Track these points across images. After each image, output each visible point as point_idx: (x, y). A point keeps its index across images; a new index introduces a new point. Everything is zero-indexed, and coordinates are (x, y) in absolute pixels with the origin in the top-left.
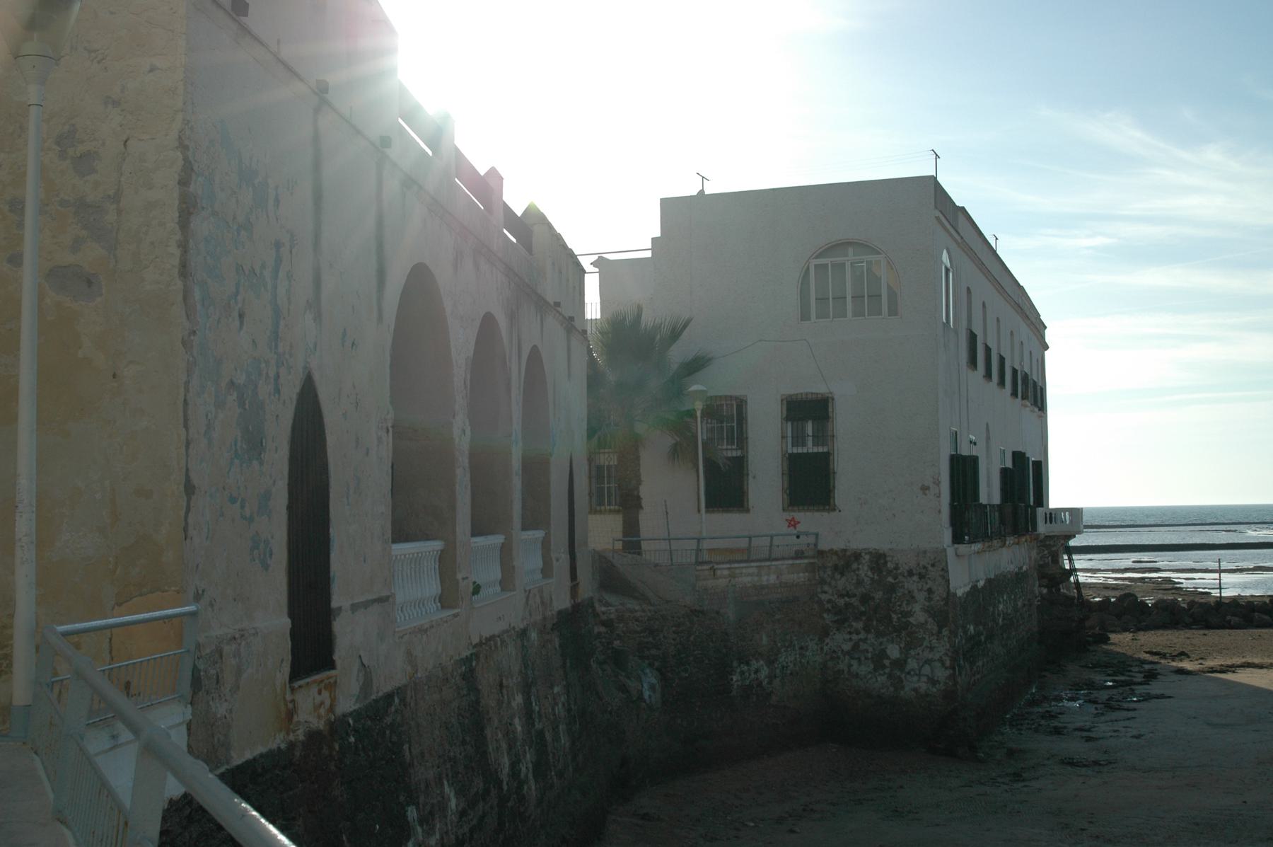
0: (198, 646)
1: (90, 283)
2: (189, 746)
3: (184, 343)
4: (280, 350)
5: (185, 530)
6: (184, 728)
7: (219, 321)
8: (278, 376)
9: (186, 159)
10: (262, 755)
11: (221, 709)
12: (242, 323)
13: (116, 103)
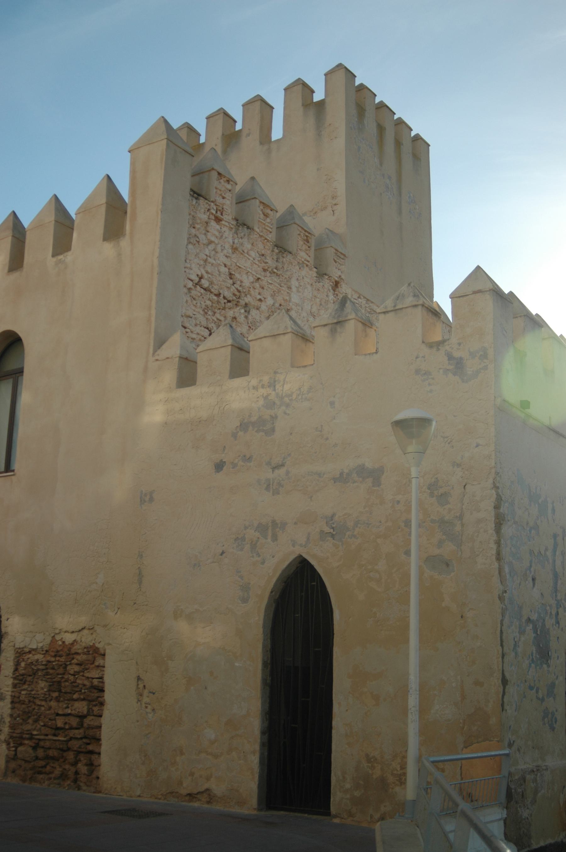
0: (510, 774)
1: (448, 565)
2: (505, 834)
3: (500, 598)
4: (559, 598)
5: (502, 705)
6: (502, 823)
7: (520, 584)
8: (557, 614)
9: (498, 494)
10: (551, 845)
11: (525, 814)
12: (534, 584)
13: (459, 465)
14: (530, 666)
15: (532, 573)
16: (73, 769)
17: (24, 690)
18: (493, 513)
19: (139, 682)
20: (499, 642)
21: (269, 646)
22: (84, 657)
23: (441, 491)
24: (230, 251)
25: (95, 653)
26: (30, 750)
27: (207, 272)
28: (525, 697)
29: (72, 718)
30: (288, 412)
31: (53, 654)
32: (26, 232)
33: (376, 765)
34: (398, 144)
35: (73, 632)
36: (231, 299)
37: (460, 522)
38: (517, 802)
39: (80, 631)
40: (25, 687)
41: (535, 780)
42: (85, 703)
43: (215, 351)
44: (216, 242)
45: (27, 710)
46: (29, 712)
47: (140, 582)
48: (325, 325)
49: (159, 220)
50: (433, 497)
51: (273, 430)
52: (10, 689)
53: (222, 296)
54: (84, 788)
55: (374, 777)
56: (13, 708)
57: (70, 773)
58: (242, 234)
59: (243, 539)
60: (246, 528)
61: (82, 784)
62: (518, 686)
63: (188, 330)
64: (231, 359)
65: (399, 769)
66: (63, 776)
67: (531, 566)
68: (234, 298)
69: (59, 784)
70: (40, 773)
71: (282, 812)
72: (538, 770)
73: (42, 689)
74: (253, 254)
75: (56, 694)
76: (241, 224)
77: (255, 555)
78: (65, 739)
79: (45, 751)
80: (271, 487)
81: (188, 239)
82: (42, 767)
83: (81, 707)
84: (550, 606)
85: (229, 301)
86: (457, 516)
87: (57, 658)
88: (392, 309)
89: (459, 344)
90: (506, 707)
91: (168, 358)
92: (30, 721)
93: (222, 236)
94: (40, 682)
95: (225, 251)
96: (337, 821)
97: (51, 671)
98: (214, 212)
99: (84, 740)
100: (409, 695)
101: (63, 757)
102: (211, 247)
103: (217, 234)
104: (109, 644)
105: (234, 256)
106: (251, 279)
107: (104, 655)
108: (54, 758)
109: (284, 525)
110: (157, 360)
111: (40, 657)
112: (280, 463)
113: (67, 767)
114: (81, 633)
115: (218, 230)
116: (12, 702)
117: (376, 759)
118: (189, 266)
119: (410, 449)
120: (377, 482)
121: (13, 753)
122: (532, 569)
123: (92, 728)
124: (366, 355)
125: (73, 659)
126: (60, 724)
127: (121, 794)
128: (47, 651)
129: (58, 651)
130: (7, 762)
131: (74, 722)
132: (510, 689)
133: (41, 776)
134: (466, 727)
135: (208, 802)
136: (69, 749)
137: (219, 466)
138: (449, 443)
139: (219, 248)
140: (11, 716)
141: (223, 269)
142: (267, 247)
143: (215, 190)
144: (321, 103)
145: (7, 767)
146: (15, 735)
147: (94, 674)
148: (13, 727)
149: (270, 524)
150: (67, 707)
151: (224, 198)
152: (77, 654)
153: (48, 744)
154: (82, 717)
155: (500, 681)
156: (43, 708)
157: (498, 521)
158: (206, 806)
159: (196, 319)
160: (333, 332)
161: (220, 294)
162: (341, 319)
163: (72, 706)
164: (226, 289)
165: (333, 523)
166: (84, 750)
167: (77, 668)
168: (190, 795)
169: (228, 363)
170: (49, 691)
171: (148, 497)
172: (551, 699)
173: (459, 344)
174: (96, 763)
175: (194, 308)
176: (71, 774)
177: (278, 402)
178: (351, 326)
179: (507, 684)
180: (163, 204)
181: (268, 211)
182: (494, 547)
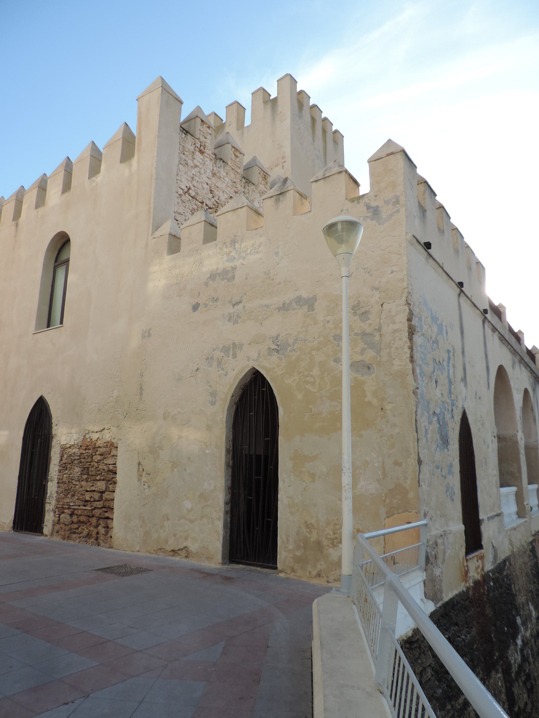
1: (369, 368)
3: (414, 393)
5: (419, 482)
6: (422, 583)
7: (427, 384)
8: (452, 410)
9: (410, 309)
10: (456, 595)
13: (377, 289)
14: (436, 450)
15: (435, 377)
16: (95, 531)
17: (65, 474)
18: (406, 324)
19: (140, 467)
20: (415, 429)
21: (231, 437)
22: (104, 449)
23: (363, 310)
24: (211, 175)
25: (112, 446)
26: (68, 517)
27: (194, 186)
28: (434, 475)
29: (95, 493)
30: (244, 263)
31: (84, 448)
32: (72, 166)
33: (313, 530)
34: (324, 131)
35: (97, 432)
36: (211, 207)
37: (378, 333)
38: (432, 564)
39: (101, 431)
40: (66, 472)
41: (443, 544)
42: (104, 482)
43: (193, 228)
44: (200, 166)
45: (67, 488)
46: (68, 490)
47: (141, 394)
48: (272, 197)
49: (157, 143)
50: (356, 315)
51: (234, 277)
52: (57, 473)
53: (205, 204)
54: (102, 544)
55: (312, 540)
56: (59, 487)
57: (93, 533)
58: (219, 165)
59: (212, 358)
60: (214, 350)
61: (101, 542)
62: (429, 466)
63: (178, 222)
64: (204, 231)
65: (332, 534)
66: (89, 535)
67: (434, 371)
68: (214, 206)
69: (86, 541)
70: (74, 533)
71: (241, 566)
72: (445, 534)
73: (77, 473)
74: (227, 179)
75: (86, 476)
76: (219, 158)
77: (220, 369)
78: (90, 508)
79: (78, 518)
80: (233, 319)
81: (179, 161)
82: (76, 529)
83: (101, 485)
84: (447, 403)
85: (210, 208)
86: (376, 329)
87: (87, 451)
88: (322, 177)
89: (376, 196)
90: (422, 483)
91: (161, 236)
92: (69, 496)
93: (204, 164)
94: (76, 468)
95: (207, 174)
96: (282, 575)
97: (83, 460)
98: (199, 146)
99: (103, 509)
100: (343, 474)
101: (89, 522)
102: (197, 169)
103: (201, 161)
104: (120, 440)
105: (213, 178)
106: (226, 196)
107: (117, 448)
108: (83, 522)
109: (241, 345)
110: (154, 238)
111: (76, 450)
112: (239, 301)
113: (91, 529)
114: (102, 432)
115: (201, 159)
116: (58, 483)
117: (313, 525)
118: (179, 179)
119: (340, 251)
120: (311, 307)
121: (57, 519)
122: (435, 374)
123: (109, 501)
124: (302, 214)
125: (97, 451)
126: (88, 498)
127: (126, 549)
128: (81, 446)
129: (87, 446)
130: (53, 525)
131: (96, 496)
132: (425, 469)
133: (75, 535)
134: (387, 501)
135: (186, 557)
136: (93, 516)
137: (195, 308)
138: (368, 273)
139: (202, 171)
140: (57, 492)
141: (205, 186)
142: (237, 177)
143: (199, 132)
144: (275, 99)
145: (53, 529)
146: (59, 506)
147: (110, 461)
148: (58, 500)
149: (231, 346)
150: (93, 486)
151: (206, 138)
152: (99, 447)
153: (79, 512)
154: (102, 492)
155: (416, 462)
156: (77, 487)
157: (410, 330)
158: (185, 560)
159: (185, 216)
160: (277, 201)
161: (203, 202)
162: (283, 191)
163: (96, 485)
164: (208, 200)
165: (278, 342)
166: (103, 516)
167: (99, 458)
168: (173, 551)
169: (202, 233)
170: (81, 474)
171: (147, 333)
172: (451, 476)
173: (376, 196)
174: (110, 526)
175: (183, 208)
176: (94, 534)
177: (237, 257)
178: (291, 196)
179: (421, 464)
180: (159, 132)
181: (238, 154)
182: (409, 351)
